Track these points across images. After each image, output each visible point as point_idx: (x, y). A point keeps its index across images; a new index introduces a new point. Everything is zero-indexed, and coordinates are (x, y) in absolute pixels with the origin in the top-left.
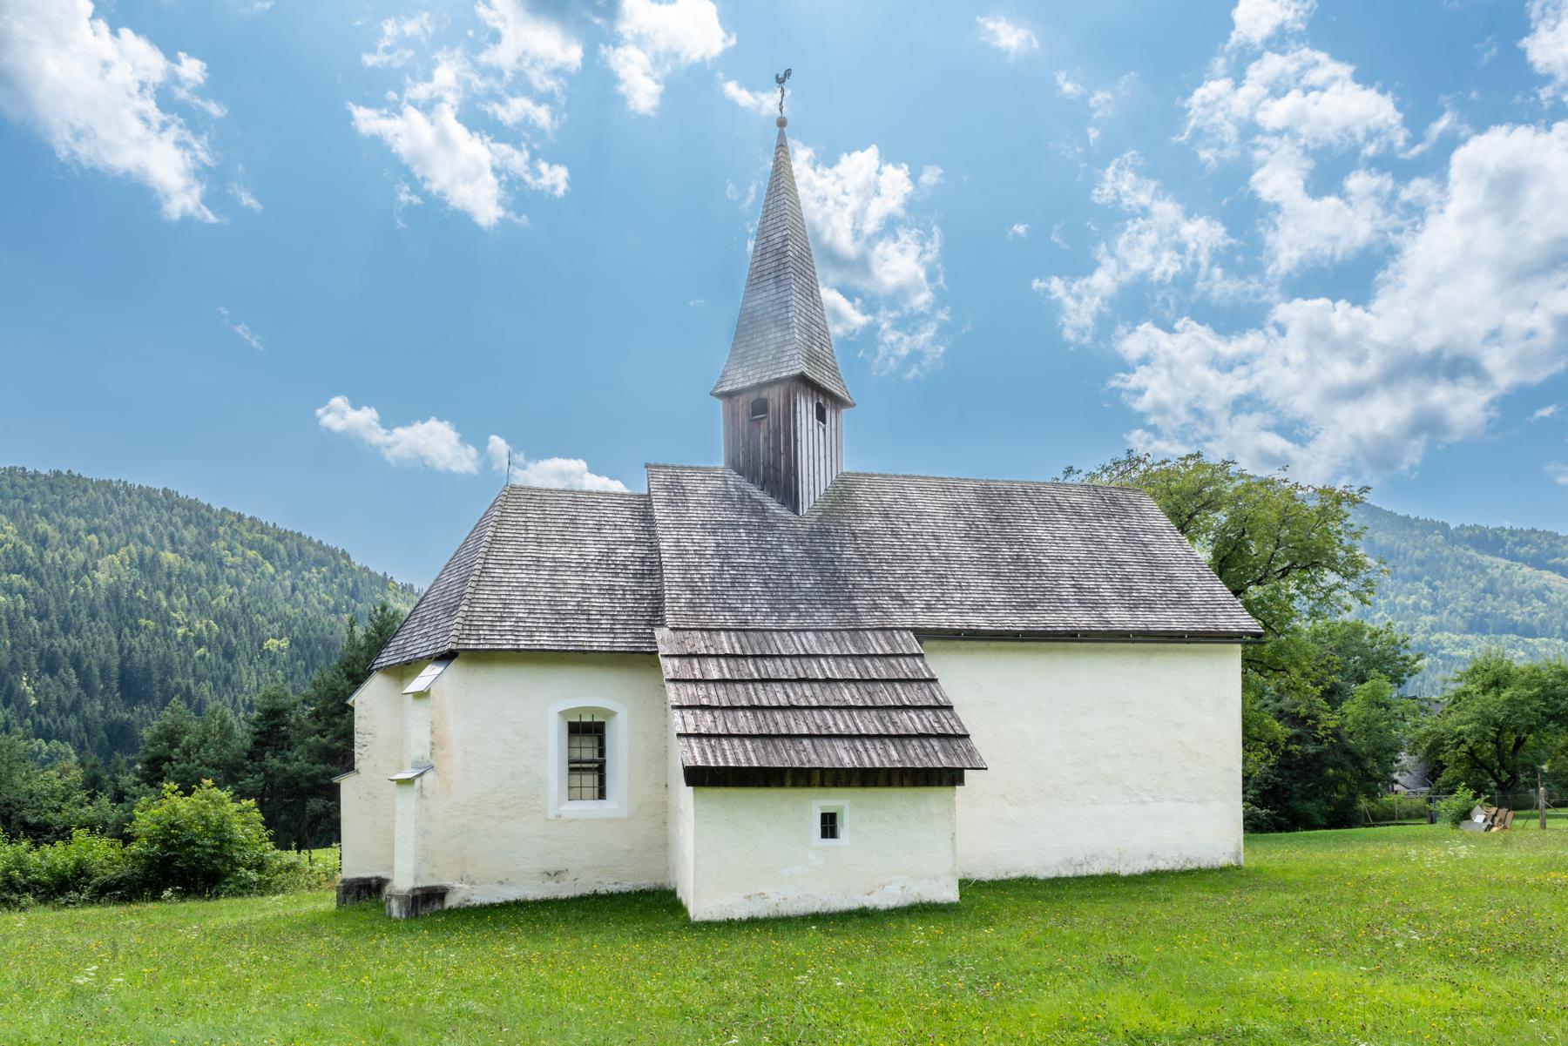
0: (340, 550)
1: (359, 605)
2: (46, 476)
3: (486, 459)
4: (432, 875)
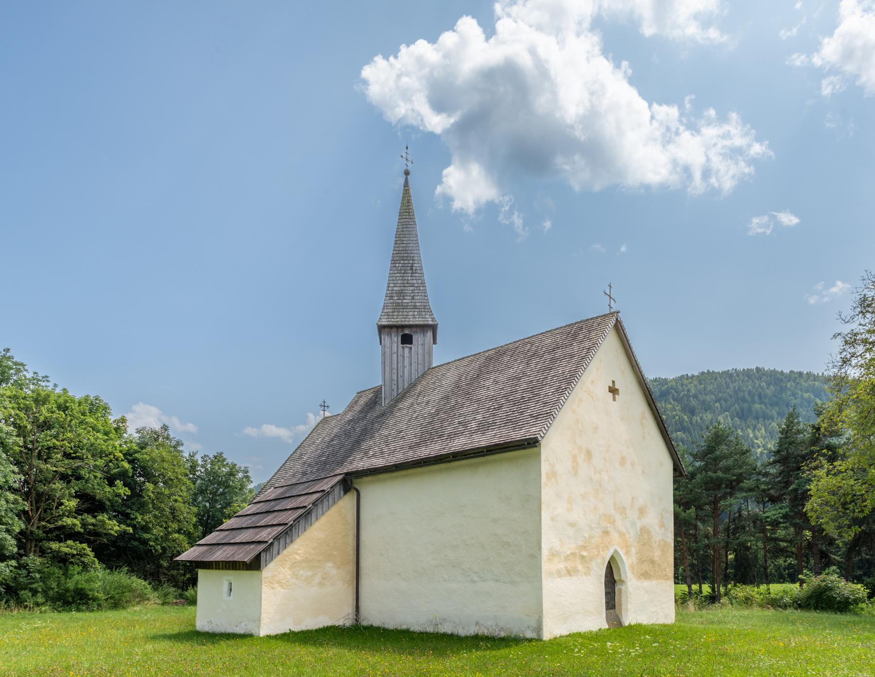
2: (697, 376)
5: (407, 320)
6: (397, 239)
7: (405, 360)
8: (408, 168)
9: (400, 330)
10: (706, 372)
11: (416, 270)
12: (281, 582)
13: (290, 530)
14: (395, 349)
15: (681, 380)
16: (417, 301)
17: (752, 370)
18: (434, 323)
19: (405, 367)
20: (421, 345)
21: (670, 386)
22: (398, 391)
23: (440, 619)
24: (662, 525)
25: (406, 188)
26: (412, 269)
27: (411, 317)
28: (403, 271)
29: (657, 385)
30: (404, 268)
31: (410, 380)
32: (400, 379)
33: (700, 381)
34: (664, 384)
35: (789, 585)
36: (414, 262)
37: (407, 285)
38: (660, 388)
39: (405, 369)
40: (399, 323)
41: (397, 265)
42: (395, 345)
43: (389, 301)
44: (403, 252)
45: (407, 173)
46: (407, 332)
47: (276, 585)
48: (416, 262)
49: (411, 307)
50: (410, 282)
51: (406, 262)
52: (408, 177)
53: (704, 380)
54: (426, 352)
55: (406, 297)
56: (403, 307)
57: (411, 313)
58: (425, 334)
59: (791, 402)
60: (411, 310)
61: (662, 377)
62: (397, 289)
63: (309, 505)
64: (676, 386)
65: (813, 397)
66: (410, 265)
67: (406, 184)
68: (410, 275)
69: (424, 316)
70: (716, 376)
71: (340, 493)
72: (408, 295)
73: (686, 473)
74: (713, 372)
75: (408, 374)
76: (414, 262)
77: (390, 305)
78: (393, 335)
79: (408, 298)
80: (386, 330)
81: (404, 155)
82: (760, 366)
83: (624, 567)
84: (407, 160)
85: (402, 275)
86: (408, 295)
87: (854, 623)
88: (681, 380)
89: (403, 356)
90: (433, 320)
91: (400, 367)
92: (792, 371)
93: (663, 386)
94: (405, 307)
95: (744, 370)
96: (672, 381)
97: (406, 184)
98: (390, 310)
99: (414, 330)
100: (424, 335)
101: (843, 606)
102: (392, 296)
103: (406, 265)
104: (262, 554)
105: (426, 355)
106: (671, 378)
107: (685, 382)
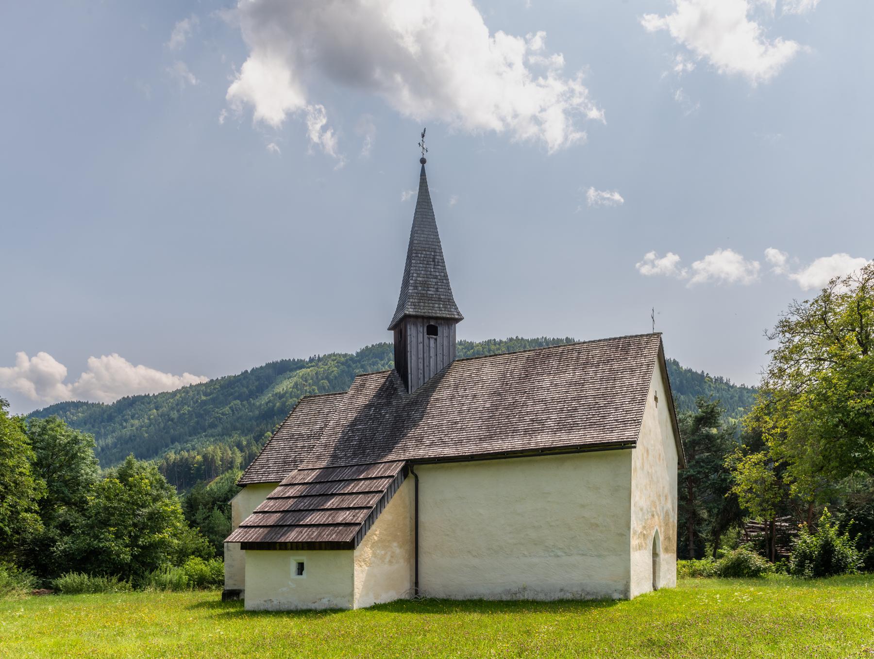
0: (672, 360)
1: (682, 396)
2: (505, 342)
3: (767, 266)
4: (235, 584)
5: (434, 311)
8: (424, 157)
10: (515, 338)
12: (366, 561)
15: (488, 345)
16: (441, 293)
17: (562, 340)
18: (459, 317)
21: (476, 351)
23: (519, 588)
24: (673, 510)
26: (434, 261)
27: (437, 309)
28: (425, 262)
29: (463, 349)
31: (436, 372)
32: (426, 369)
33: (508, 348)
34: (470, 348)
36: (436, 254)
37: (430, 276)
38: (466, 352)
40: (427, 314)
41: (419, 255)
42: (421, 335)
44: (424, 242)
45: (423, 161)
46: (432, 323)
47: (363, 563)
48: (438, 254)
49: (436, 299)
50: (433, 273)
51: (428, 253)
53: (513, 347)
54: (451, 344)
55: (430, 289)
56: (428, 299)
57: (437, 305)
60: (437, 302)
61: (467, 340)
64: (482, 351)
66: (432, 257)
70: (525, 344)
74: (522, 339)
75: (433, 365)
76: (436, 254)
78: (419, 326)
79: (433, 289)
80: (412, 319)
82: (570, 337)
83: (659, 543)
85: (424, 266)
87: (850, 579)
88: (488, 345)
91: (426, 357)
93: (469, 350)
95: (553, 339)
96: (478, 346)
98: (416, 300)
99: (440, 321)
100: (449, 328)
101: (755, 574)
103: (428, 256)
106: (477, 342)
107: (493, 347)
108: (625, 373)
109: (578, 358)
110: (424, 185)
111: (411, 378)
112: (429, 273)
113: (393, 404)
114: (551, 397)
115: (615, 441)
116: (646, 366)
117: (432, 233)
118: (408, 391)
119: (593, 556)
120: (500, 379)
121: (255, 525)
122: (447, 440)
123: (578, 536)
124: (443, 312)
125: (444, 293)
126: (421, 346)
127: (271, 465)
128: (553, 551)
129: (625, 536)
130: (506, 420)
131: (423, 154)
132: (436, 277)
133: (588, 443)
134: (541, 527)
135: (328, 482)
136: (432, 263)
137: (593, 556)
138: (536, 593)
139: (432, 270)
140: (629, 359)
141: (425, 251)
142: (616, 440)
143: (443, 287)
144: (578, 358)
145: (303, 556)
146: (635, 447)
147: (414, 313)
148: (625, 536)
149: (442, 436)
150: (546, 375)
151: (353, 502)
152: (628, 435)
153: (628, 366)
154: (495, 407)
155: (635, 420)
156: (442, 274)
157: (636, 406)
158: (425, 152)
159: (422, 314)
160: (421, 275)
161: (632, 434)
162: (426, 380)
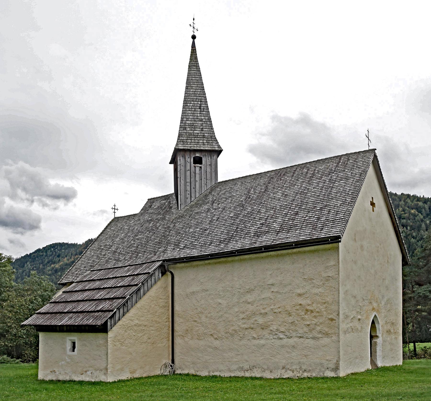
5: (198, 146)
6: (188, 85)
7: (197, 176)
8: (195, 34)
9: (192, 153)
11: (203, 109)
13: (126, 302)
14: (188, 168)
16: (205, 132)
19: (196, 181)
20: (209, 166)
22: (191, 199)
23: (250, 366)
25: (193, 49)
27: (201, 144)
28: (193, 110)
30: (194, 107)
35: (217, 374)
39: (197, 183)
40: (192, 148)
41: (189, 105)
42: (189, 164)
43: (183, 131)
45: (194, 37)
46: (198, 155)
49: (201, 137)
51: (196, 103)
52: (195, 40)
54: (213, 170)
55: (196, 129)
56: (195, 136)
57: (201, 141)
58: (212, 156)
59: (402, 215)
60: (201, 139)
62: (189, 122)
63: (139, 284)
65: (417, 213)
66: (199, 105)
67: (194, 43)
68: (199, 112)
69: (211, 144)
71: (159, 275)
72: (198, 127)
73: (410, 263)
77: (184, 134)
79: (198, 129)
80: (182, 153)
81: (192, 24)
84: (194, 28)
85: (193, 112)
86: (198, 127)
89: (195, 173)
90: (219, 146)
92: (403, 193)
94: (196, 136)
97: (194, 43)
99: (204, 154)
102: (185, 128)
103: (195, 105)
104: (108, 320)
105: (213, 173)
108: (341, 182)
109: (307, 173)
110: (194, 54)
111: (181, 198)
112: (195, 117)
113: (166, 218)
114: (280, 205)
115: (323, 236)
116: (359, 175)
117: (200, 88)
118: (178, 209)
119: (309, 338)
120: (245, 194)
121: (64, 314)
122: (196, 243)
123: (296, 321)
124: (206, 146)
125: (208, 132)
126: (188, 173)
127: (82, 269)
128: (276, 334)
129: (335, 320)
130: (242, 226)
131: (194, 32)
132: (201, 120)
133: (301, 240)
134: (266, 313)
135: (105, 279)
136: (198, 110)
137: (309, 338)
138: (263, 370)
139: (199, 115)
140: (346, 171)
141: (193, 101)
142: (324, 236)
143: (207, 127)
144: (307, 173)
145: (75, 337)
146: (340, 241)
147: (182, 148)
148: (335, 320)
149: (194, 240)
150: (280, 188)
151: (115, 293)
152: (334, 233)
153: (344, 176)
154: (237, 216)
155: (343, 219)
156: (207, 118)
157: (346, 207)
158: (195, 31)
159: (189, 148)
160: (189, 119)
161: (338, 230)
162: (192, 199)
